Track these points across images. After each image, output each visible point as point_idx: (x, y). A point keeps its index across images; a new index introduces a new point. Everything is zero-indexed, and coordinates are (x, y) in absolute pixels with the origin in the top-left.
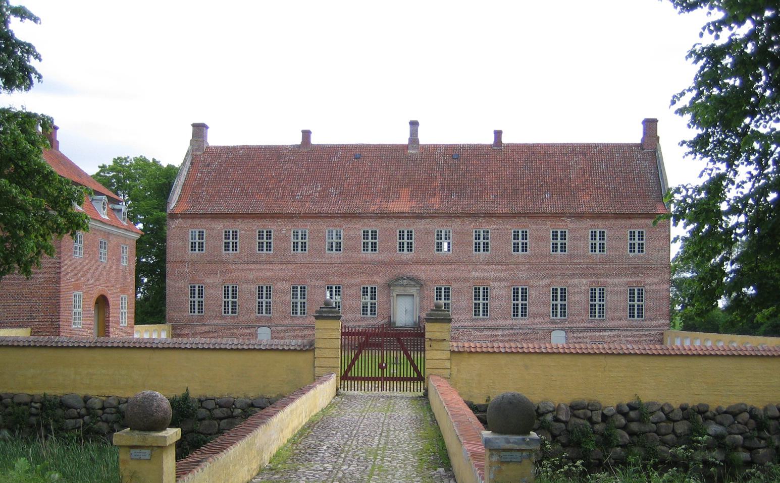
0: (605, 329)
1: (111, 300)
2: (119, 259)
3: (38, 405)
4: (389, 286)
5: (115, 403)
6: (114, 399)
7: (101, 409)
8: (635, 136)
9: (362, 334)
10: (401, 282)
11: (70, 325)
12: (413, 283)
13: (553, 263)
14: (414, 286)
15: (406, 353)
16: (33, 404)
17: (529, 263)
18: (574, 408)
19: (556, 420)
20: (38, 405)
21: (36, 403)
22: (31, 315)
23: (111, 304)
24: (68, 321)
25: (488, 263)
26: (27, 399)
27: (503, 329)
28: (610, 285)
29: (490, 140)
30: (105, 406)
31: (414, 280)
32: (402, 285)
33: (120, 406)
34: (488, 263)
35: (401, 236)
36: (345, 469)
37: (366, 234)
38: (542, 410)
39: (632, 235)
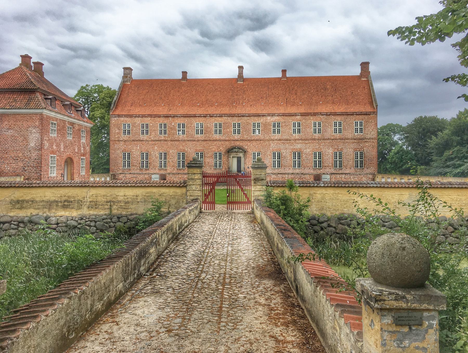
0: (342, 174)
1: (75, 160)
2: (80, 138)
3: (15, 223)
4: (228, 152)
5: (64, 220)
6: (64, 218)
7: (56, 224)
8: (357, 71)
9: (215, 177)
10: (235, 150)
11: (48, 174)
12: (241, 151)
13: (314, 139)
14: (241, 152)
15: (240, 186)
16: (12, 222)
17: (301, 139)
18: (340, 219)
19: (329, 226)
20: (15, 223)
21: (14, 221)
22: (24, 169)
23: (75, 163)
24: (47, 171)
25: (280, 140)
26: (9, 219)
27: (288, 174)
28: (345, 151)
29: (280, 75)
30: (59, 222)
31: (241, 149)
32: (235, 152)
33: (68, 222)
34: (280, 140)
35: (234, 126)
36: (204, 278)
37: (216, 125)
38: (321, 220)
39: (356, 124)
